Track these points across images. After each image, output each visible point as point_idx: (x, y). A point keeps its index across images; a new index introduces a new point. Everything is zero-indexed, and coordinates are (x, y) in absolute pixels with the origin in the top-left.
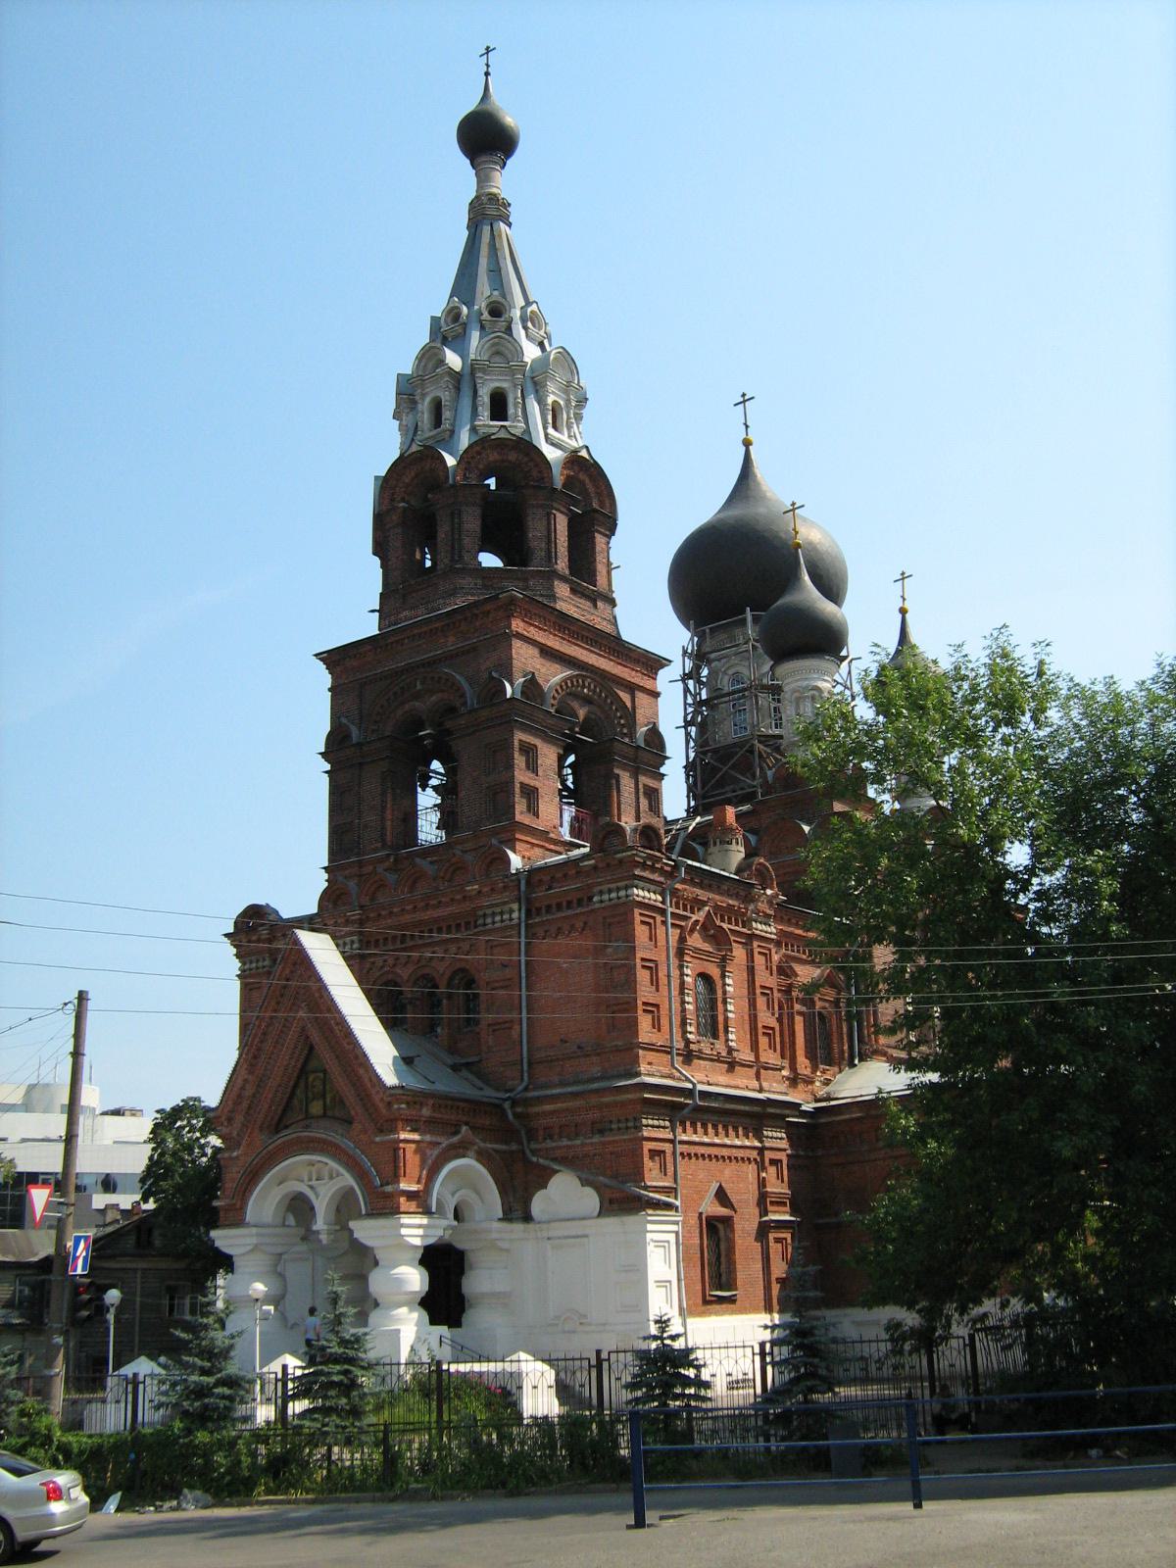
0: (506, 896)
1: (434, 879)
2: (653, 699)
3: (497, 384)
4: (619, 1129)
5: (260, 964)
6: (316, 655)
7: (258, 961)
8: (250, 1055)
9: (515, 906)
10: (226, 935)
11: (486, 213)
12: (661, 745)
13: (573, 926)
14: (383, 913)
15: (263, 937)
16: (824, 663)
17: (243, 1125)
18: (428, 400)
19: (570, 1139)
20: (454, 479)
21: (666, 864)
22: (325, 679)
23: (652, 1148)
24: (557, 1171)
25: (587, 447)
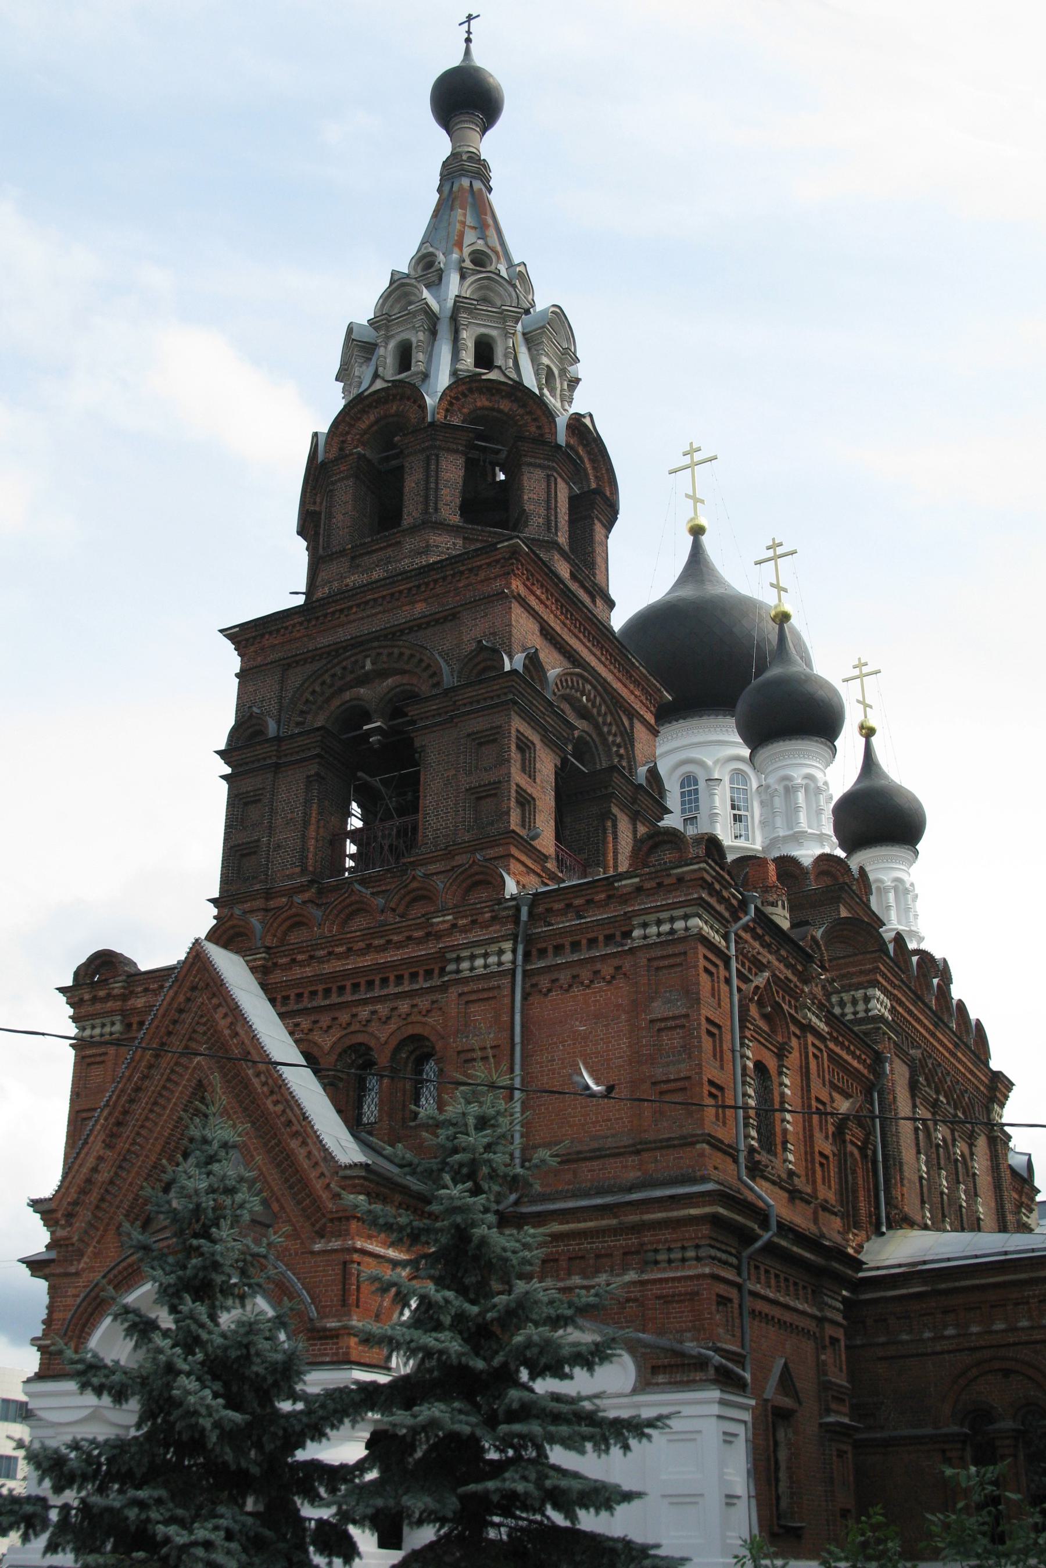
0: (494, 931)
1: (382, 911)
2: (651, 737)
3: (483, 330)
4: (670, 1261)
5: (107, 1029)
6: (221, 631)
7: (103, 1025)
8: (112, 1120)
9: (508, 945)
10: (61, 990)
11: (464, 181)
12: (661, 790)
14: (300, 957)
15: (116, 992)
16: (813, 746)
17: (90, 1224)
18: (392, 345)
19: (585, 1277)
20: (433, 415)
21: (734, 896)
22: (231, 661)
23: (721, 1292)
25: (591, 415)
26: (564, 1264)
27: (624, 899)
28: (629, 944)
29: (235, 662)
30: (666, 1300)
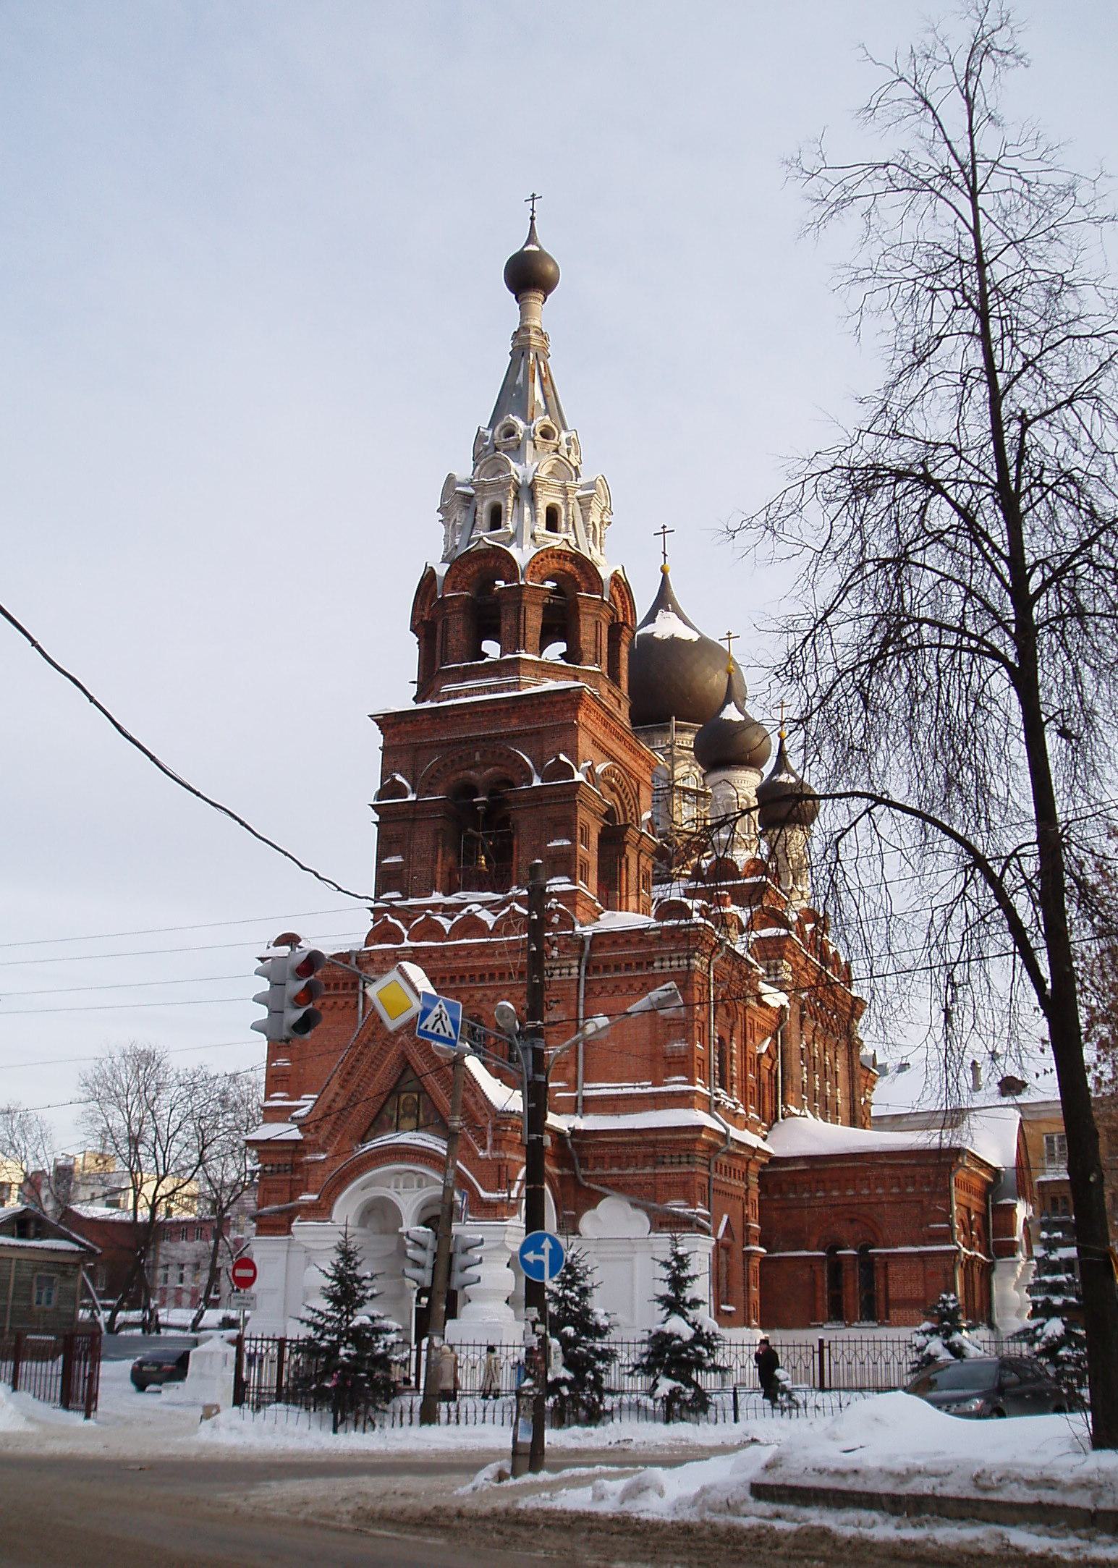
11: (522, 347)
13: (631, 986)
18: (486, 504)
19: (621, 1168)
22: (377, 738)
24: (607, 1196)
26: (607, 1160)
27: (651, 944)
28: (651, 971)
29: (379, 739)
30: (668, 1184)
